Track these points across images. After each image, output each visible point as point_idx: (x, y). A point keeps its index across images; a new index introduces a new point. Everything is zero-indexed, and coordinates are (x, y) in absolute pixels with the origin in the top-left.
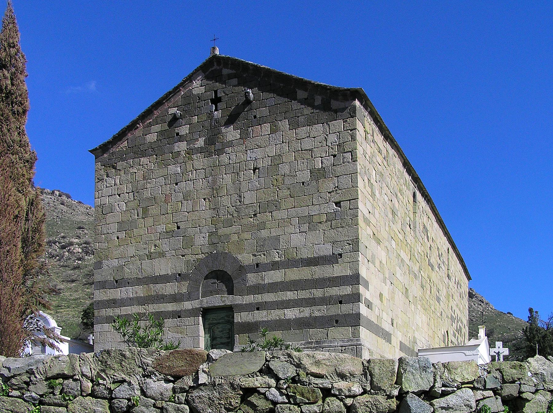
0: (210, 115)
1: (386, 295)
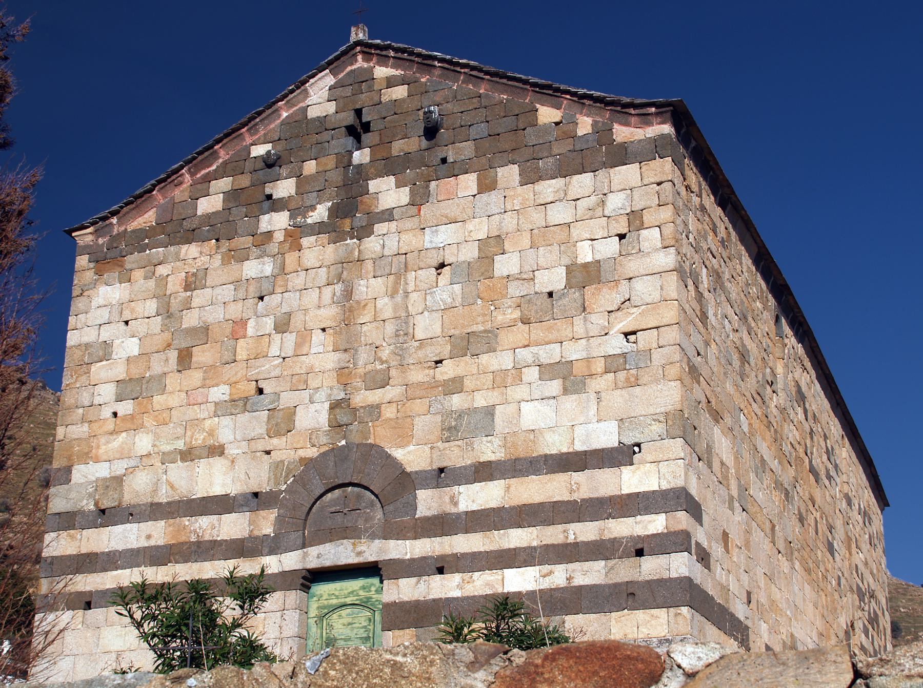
0: (345, 161)
1: (736, 538)
